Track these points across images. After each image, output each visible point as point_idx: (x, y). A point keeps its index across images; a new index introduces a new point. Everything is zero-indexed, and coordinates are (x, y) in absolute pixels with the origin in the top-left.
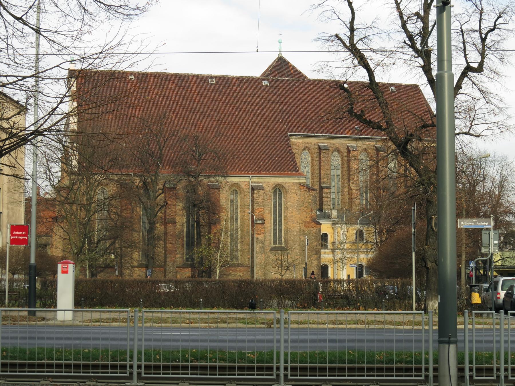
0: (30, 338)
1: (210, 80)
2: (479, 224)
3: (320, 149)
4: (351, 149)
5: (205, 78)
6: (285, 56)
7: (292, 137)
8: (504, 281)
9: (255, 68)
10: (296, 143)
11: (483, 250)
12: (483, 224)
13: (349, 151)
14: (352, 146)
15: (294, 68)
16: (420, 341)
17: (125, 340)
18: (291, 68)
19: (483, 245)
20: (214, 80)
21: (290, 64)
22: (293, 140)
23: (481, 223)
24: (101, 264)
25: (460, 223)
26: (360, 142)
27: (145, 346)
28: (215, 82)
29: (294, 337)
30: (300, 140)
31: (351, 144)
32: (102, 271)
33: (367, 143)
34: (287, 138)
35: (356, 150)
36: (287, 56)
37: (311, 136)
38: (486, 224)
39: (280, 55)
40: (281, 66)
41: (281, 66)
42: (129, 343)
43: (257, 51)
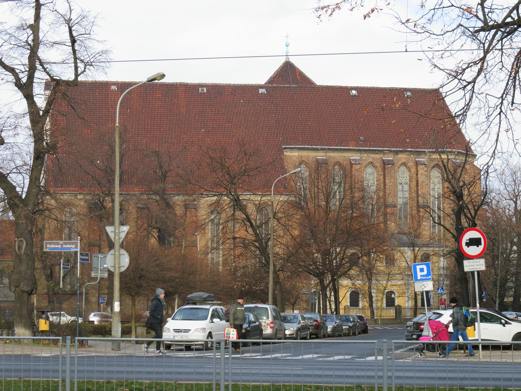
0: (48, 371)
1: (200, 89)
2: (65, 246)
3: (385, 163)
4: (353, 162)
5: (195, 87)
6: (292, 60)
7: (287, 150)
8: (267, 309)
9: (258, 74)
10: (292, 157)
11: (93, 275)
12: (70, 246)
13: (352, 165)
14: (355, 160)
15: (301, 74)
16: (58, 371)
17: (211, 374)
18: (297, 74)
19: (93, 269)
20: (205, 89)
21: (298, 69)
22: (287, 153)
23: (68, 246)
24: (68, 291)
25: (46, 246)
26: (365, 155)
27: (396, 384)
28: (205, 91)
29: (81, 368)
30: (295, 154)
31: (355, 156)
32: (67, 299)
33: (373, 156)
34: (281, 151)
35: (358, 164)
36: (294, 60)
37: (308, 149)
38: (73, 246)
39: (287, 60)
40: (288, 72)
41: (288, 72)
42: (213, 377)
43: (406, 51)
